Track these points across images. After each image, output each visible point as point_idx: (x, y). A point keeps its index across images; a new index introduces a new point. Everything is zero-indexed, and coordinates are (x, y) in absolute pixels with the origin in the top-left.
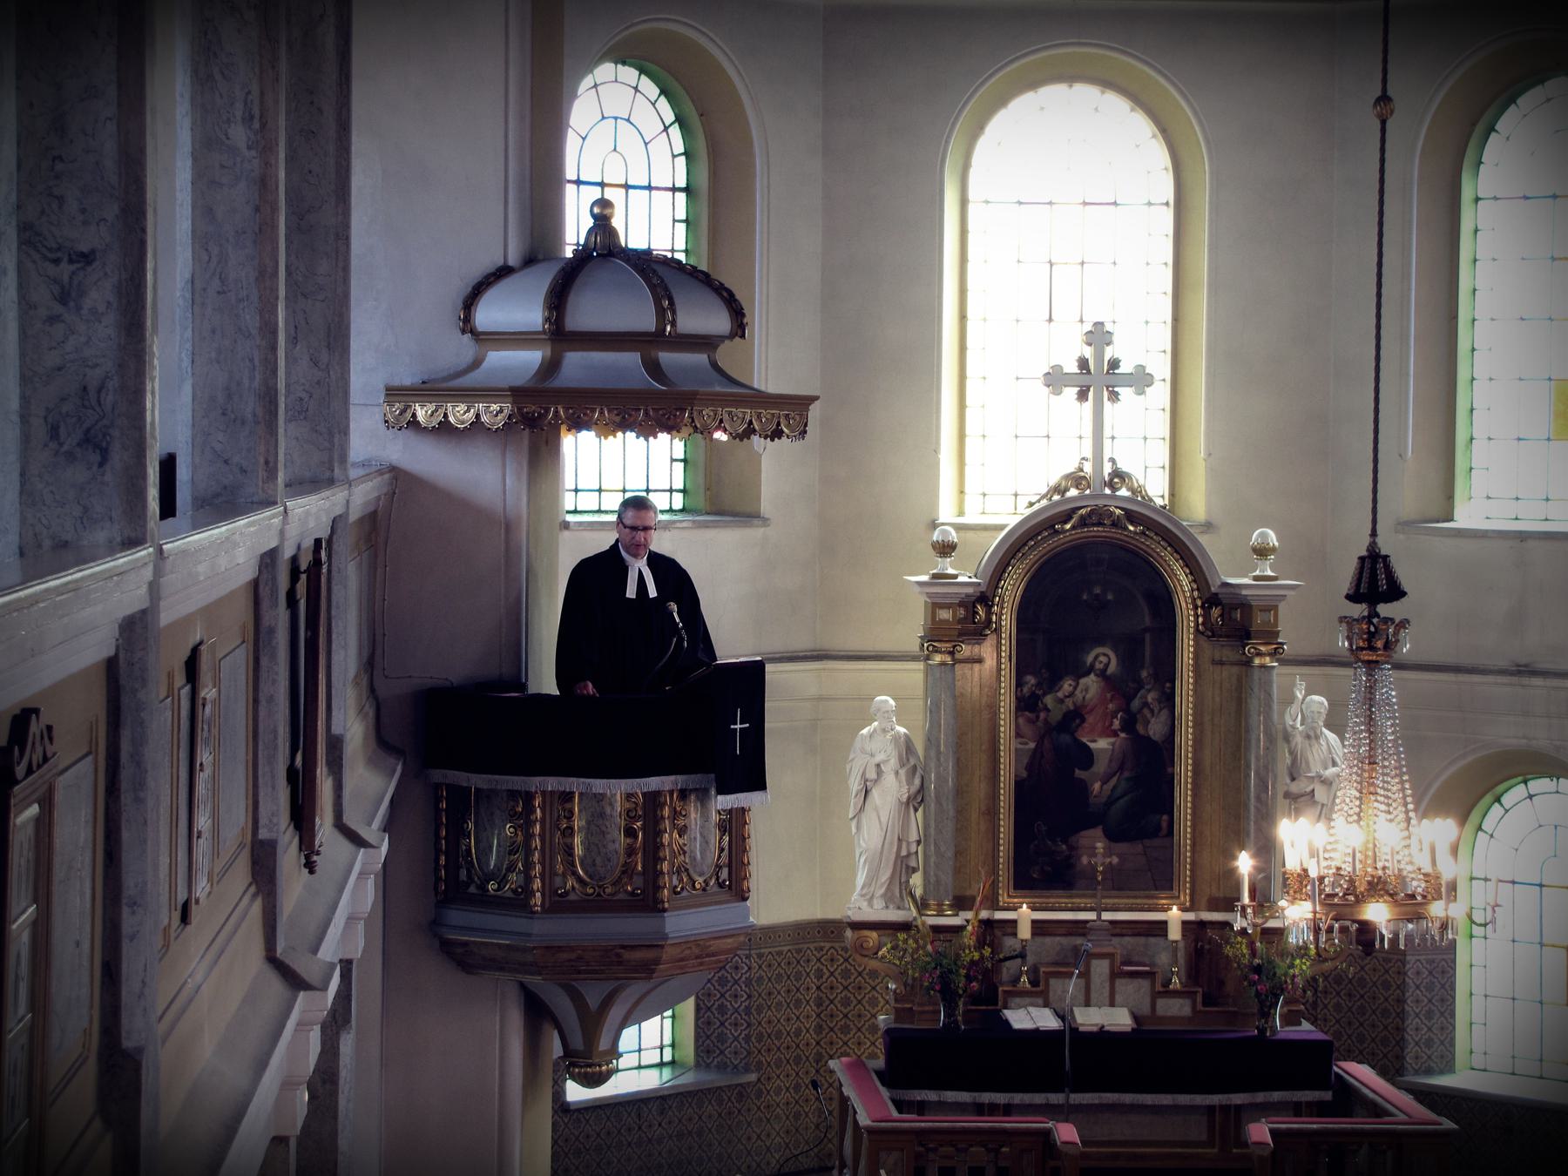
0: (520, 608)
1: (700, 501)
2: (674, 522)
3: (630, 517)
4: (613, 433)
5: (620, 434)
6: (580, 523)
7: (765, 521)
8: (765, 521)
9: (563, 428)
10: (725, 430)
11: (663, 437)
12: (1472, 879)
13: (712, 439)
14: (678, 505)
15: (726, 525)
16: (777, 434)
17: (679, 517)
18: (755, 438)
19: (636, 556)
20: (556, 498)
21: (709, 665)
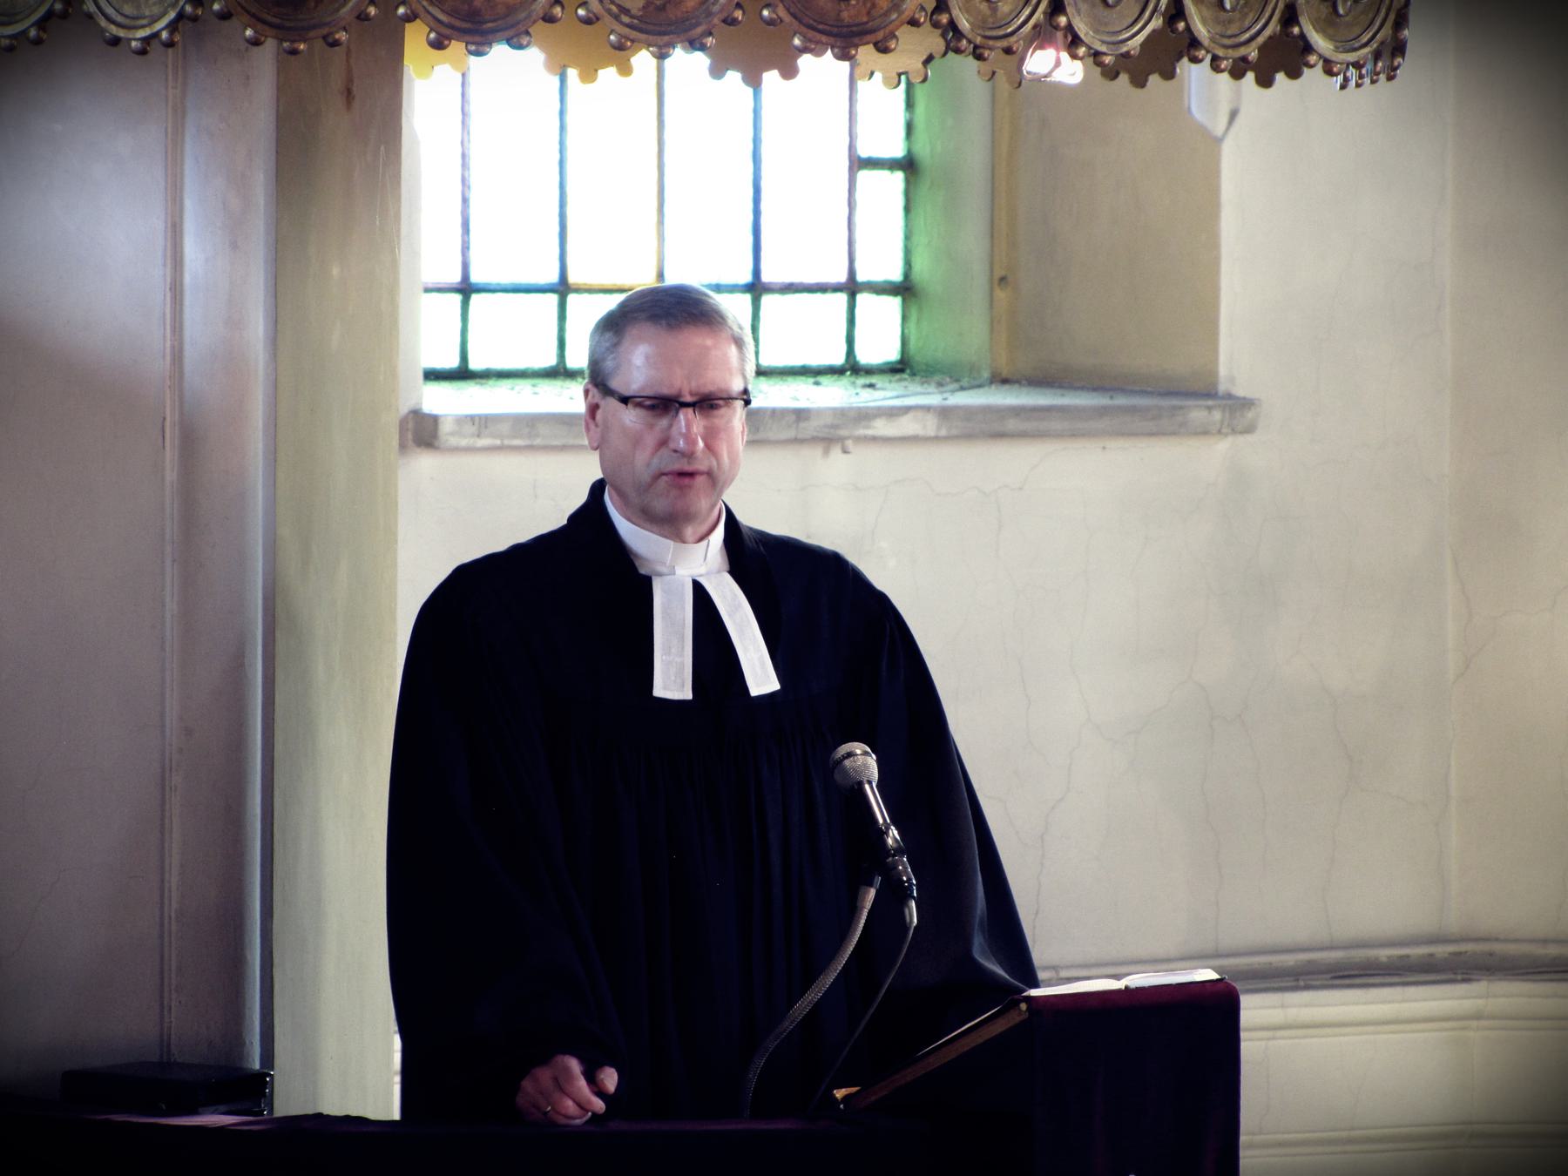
0: (237, 745)
1: (967, 332)
2: (864, 416)
3: (639, 366)
4: (620, 53)
5: (643, 60)
6: (482, 423)
7: (1237, 412)
8: (1237, 412)
9: (416, 38)
10: (1073, 42)
11: (822, 71)
12: (859, 163)
13: (1018, 81)
14: (880, 346)
15: (1074, 427)
16: (1283, 57)
17: (888, 394)
18: (1194, 74)
19: (672, 523)
20: (381, 323)
21: (1007, 996)
